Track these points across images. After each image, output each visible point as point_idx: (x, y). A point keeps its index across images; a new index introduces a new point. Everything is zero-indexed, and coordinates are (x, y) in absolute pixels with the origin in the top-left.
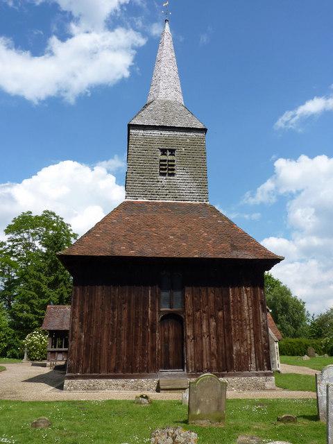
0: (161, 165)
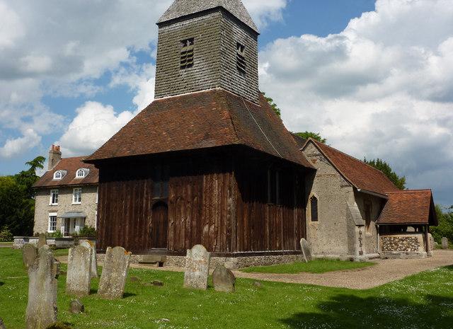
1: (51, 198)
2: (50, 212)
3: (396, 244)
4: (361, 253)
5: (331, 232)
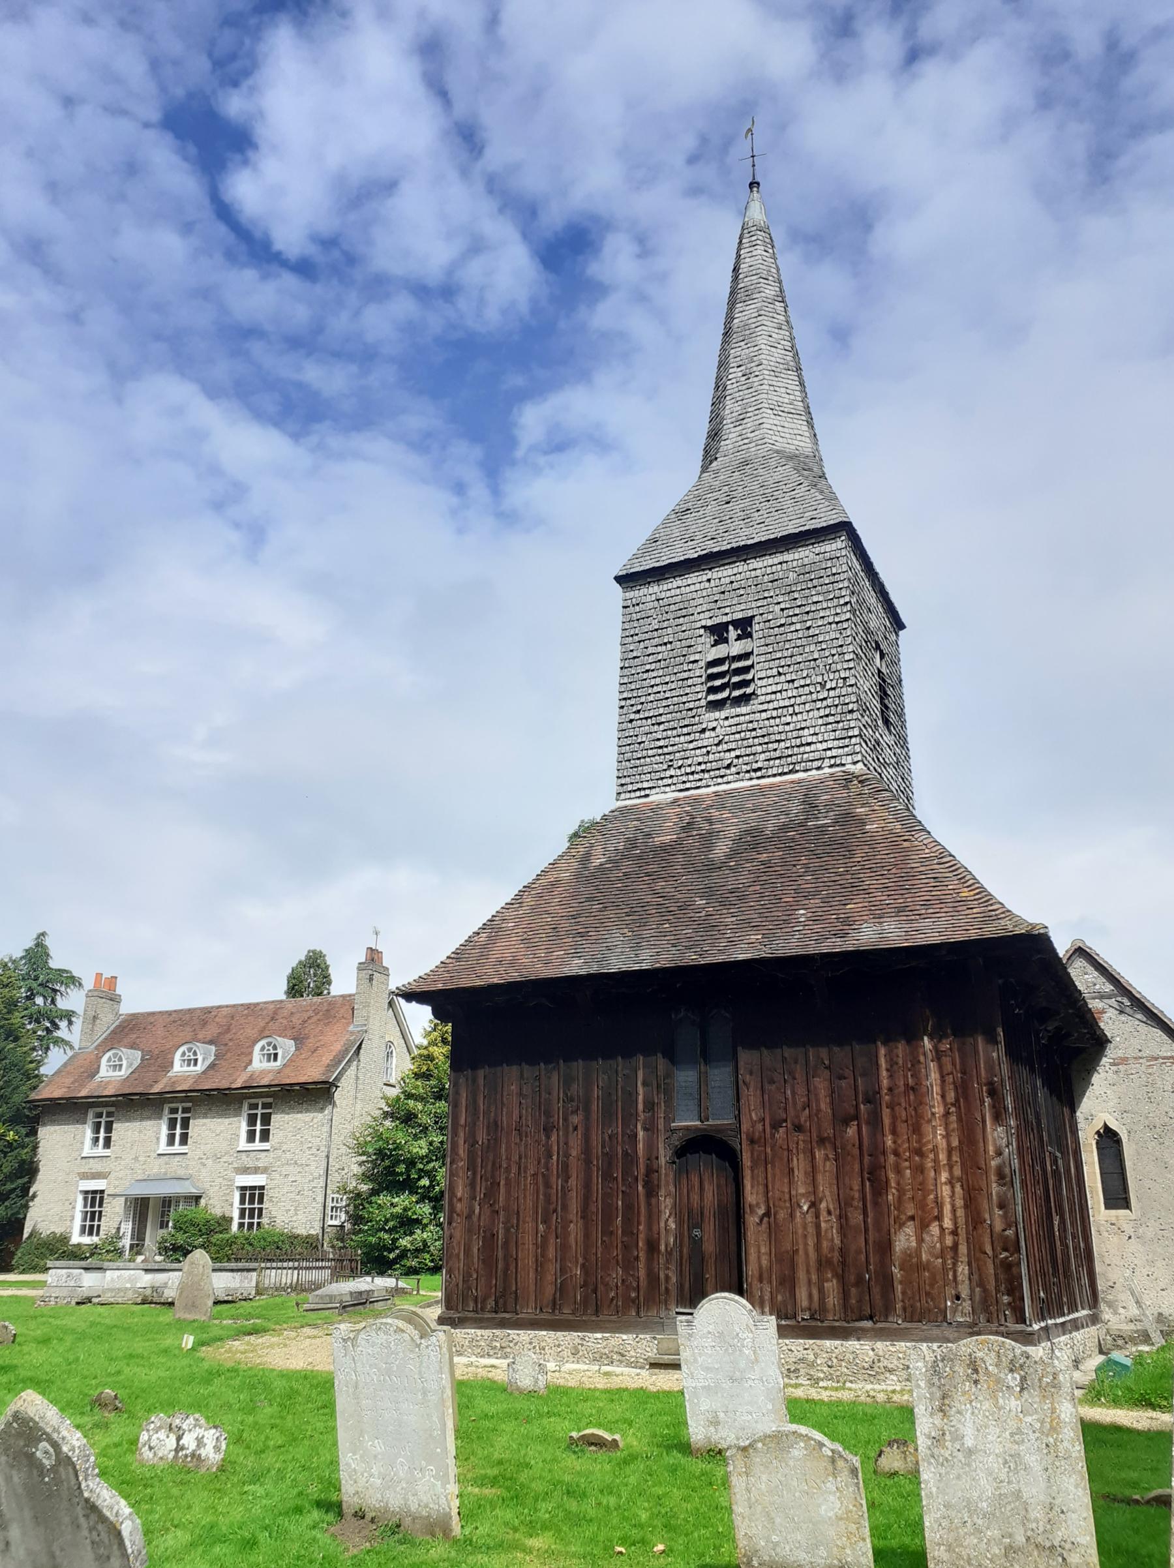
0: (712, 677)
1: (244, 1127)
2: (85, 1176)
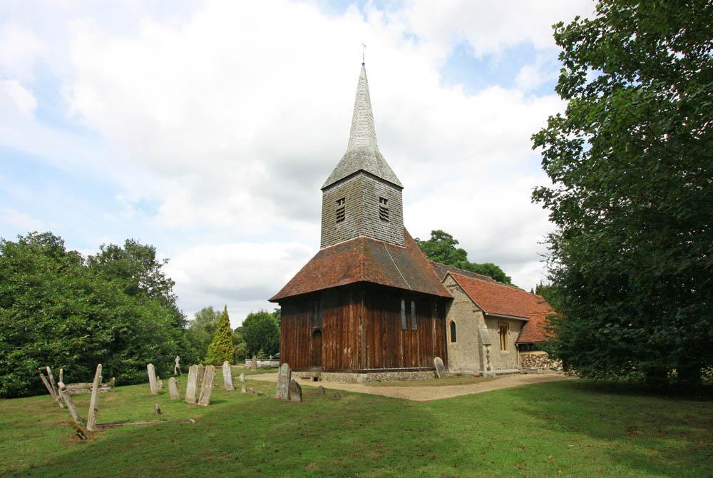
3: (534, 361)
4: (489, 369)
5: (467, 351)
